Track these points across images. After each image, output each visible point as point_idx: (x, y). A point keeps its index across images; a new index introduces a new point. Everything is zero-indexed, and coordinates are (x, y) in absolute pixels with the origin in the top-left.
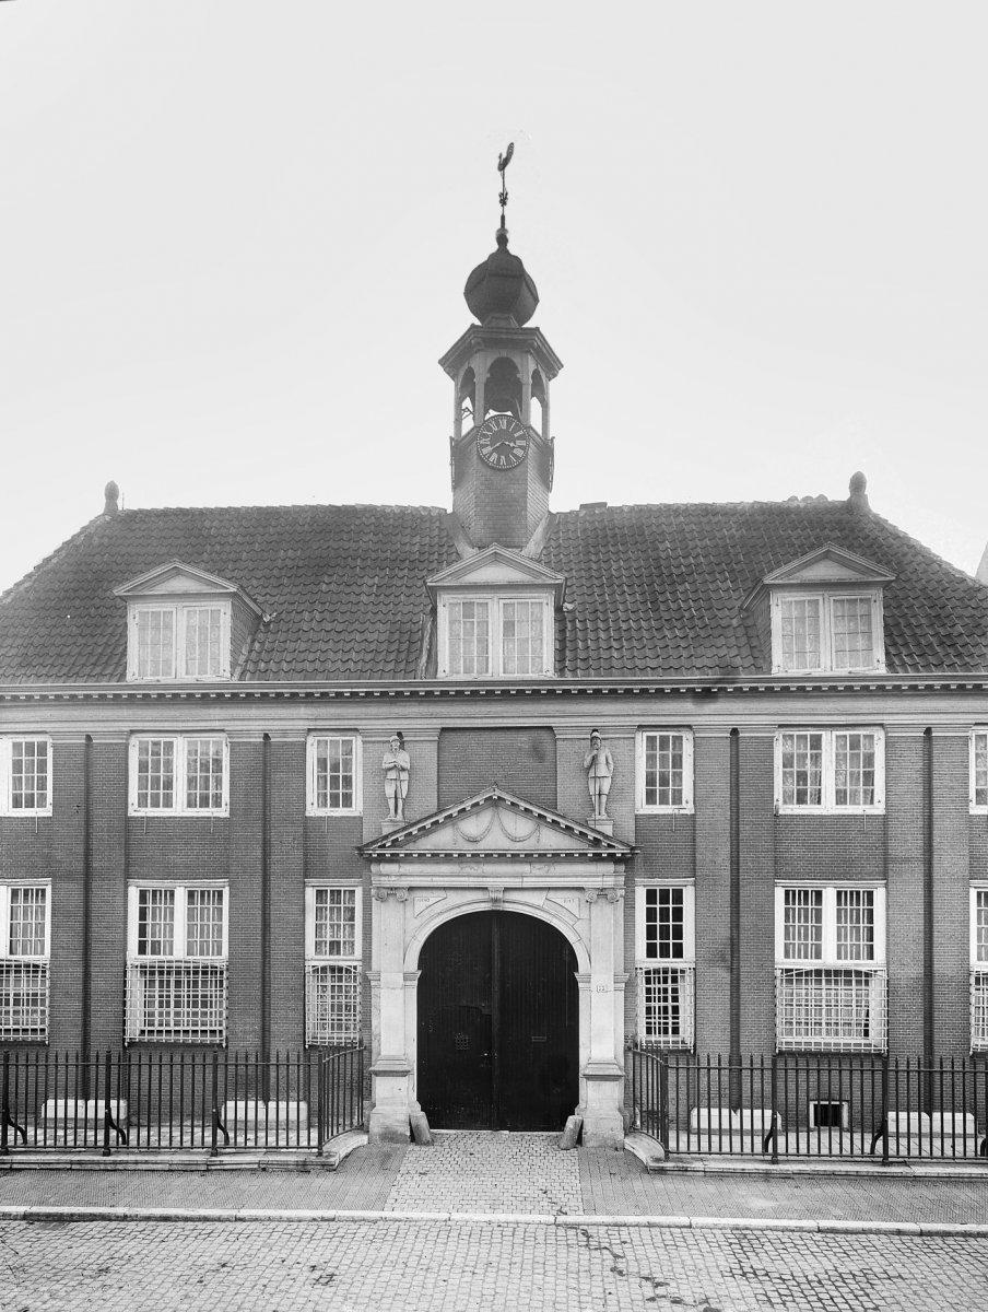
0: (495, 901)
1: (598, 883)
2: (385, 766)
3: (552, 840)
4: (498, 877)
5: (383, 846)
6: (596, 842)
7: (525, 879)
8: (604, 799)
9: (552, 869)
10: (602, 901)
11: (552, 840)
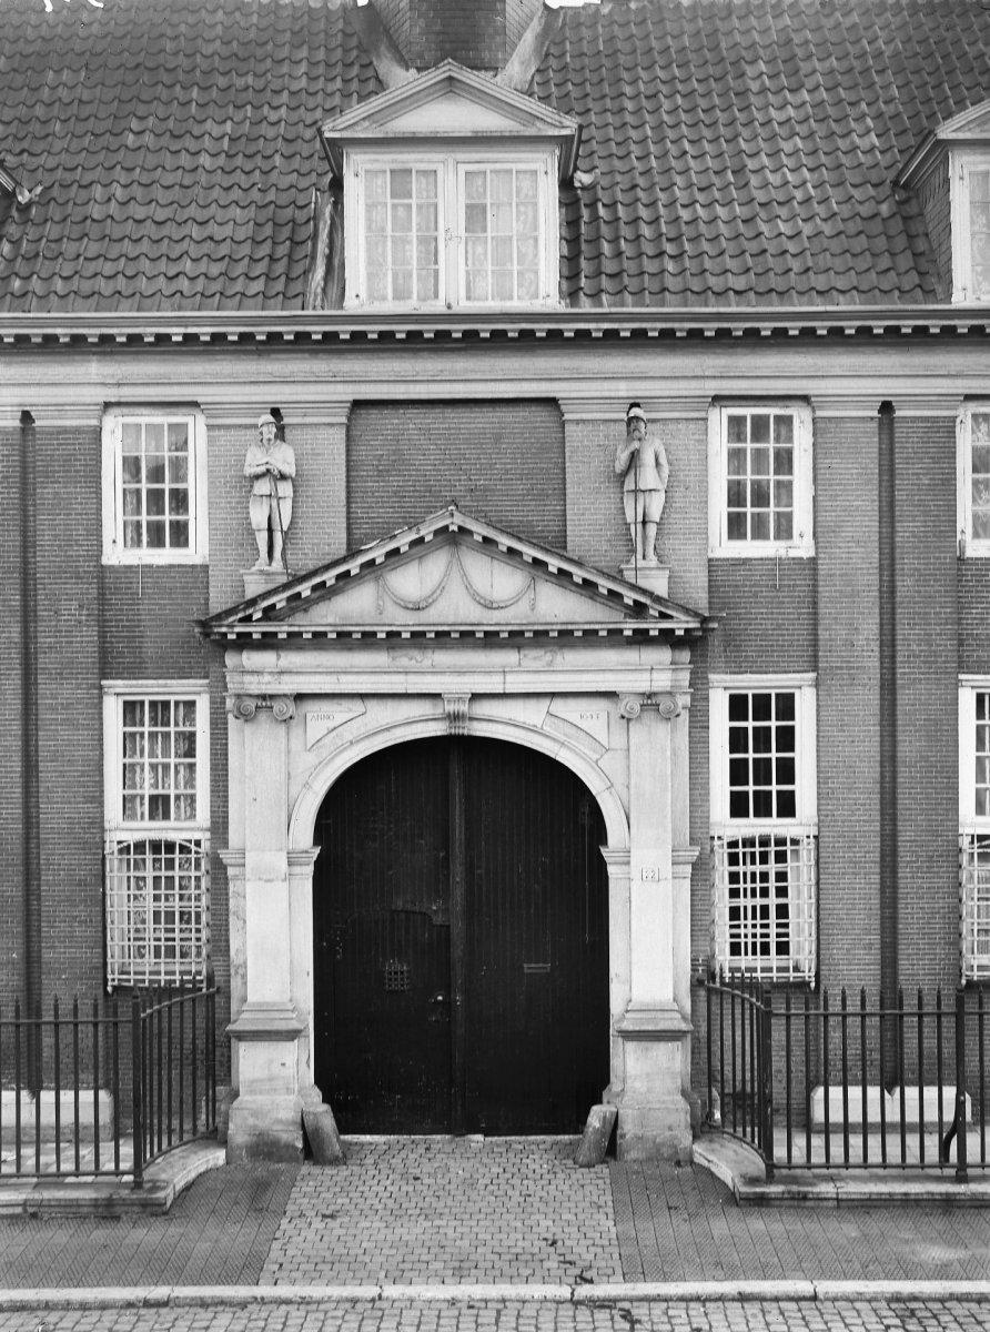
0: (455, 718)
1: (642, 683)
2: (249, 471)
3: (558, 607)
4: (456, 675)
5: (248, 619)
6: (639, 610)
7: (509, 678)
8: (652, 530)
9: (559, 658)
10: (649, 716)
11: (558, 607)
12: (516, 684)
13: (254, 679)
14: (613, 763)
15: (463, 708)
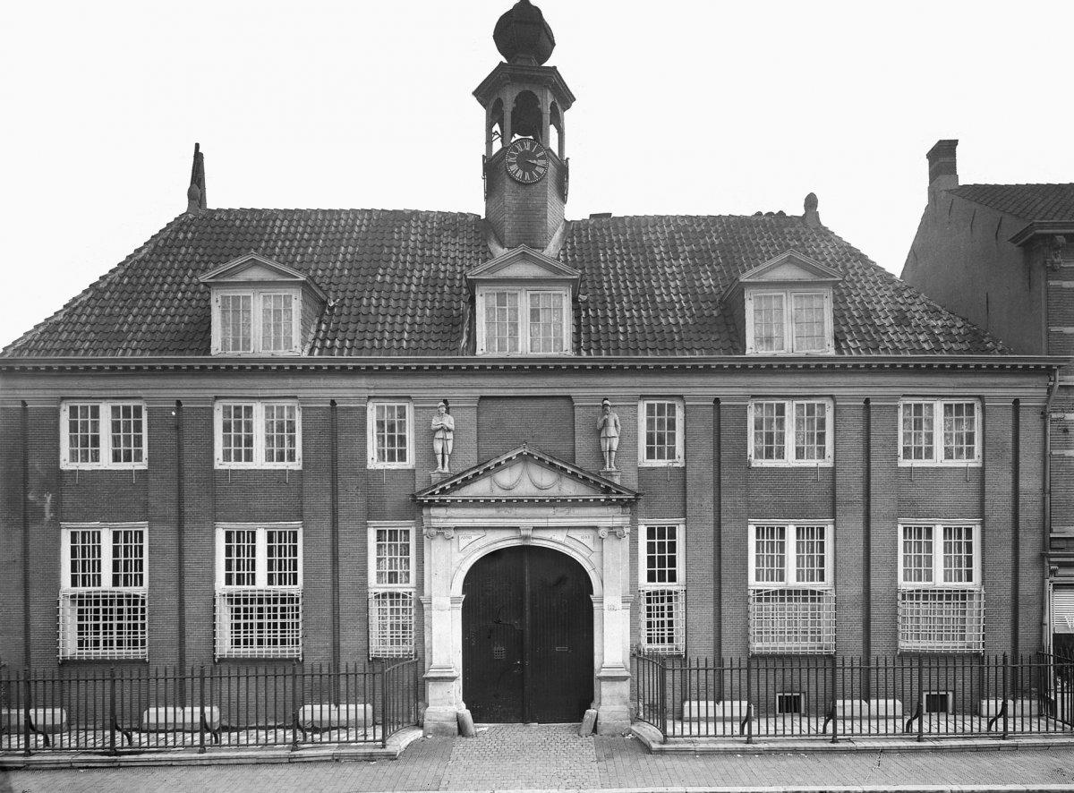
0: (526, 538)
4: (526, 519)
7: (550, 520)
11: (570, 489)
12: (553, 522)
13: (435, 520)
14: (595, 558)
15: (529, 533)
